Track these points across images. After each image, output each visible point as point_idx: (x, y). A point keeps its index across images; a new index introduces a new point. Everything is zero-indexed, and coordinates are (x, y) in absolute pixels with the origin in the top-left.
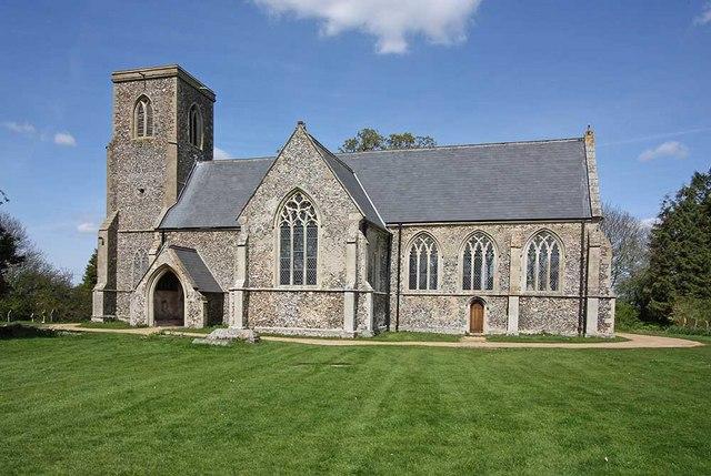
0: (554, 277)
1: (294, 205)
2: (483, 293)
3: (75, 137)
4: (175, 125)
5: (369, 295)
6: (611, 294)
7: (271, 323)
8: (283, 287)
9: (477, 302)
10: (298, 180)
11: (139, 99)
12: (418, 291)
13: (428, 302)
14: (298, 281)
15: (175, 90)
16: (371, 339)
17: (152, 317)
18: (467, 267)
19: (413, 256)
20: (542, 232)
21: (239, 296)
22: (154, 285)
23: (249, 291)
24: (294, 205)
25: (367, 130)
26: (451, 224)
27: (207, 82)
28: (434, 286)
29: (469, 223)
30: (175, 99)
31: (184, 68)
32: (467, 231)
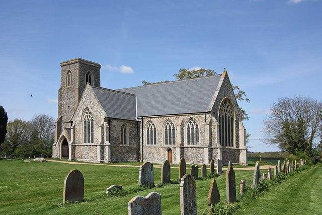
0: (197, 139)
1: (87, 113)
2: (171, 146)
3: (132, 67)
4: (78, 81)
5: (107, 147)
6: (218, 146)
7: (81, 157)
8: (84, 144)
9: (169, 150)
10: (87, 104)
11: (68, 72)
12: (150, 145)
13: (153, 150)
14: (89, 142)
15: (78, 67)
16: (108, 164)
17: (61, 156)
18: (166, 132)
19: (189, 131)
20: (191, 119)
21: (178, 150)
22: (61, 143)
23: (212, 148)
24: (87, 113)
25: (181, 69)
26: (159, 116)
27: (95, 61)
28: (155, 143)
29: (165, 116)
30: (78, 71)
31: (82, 58)
32: (164, 119)
